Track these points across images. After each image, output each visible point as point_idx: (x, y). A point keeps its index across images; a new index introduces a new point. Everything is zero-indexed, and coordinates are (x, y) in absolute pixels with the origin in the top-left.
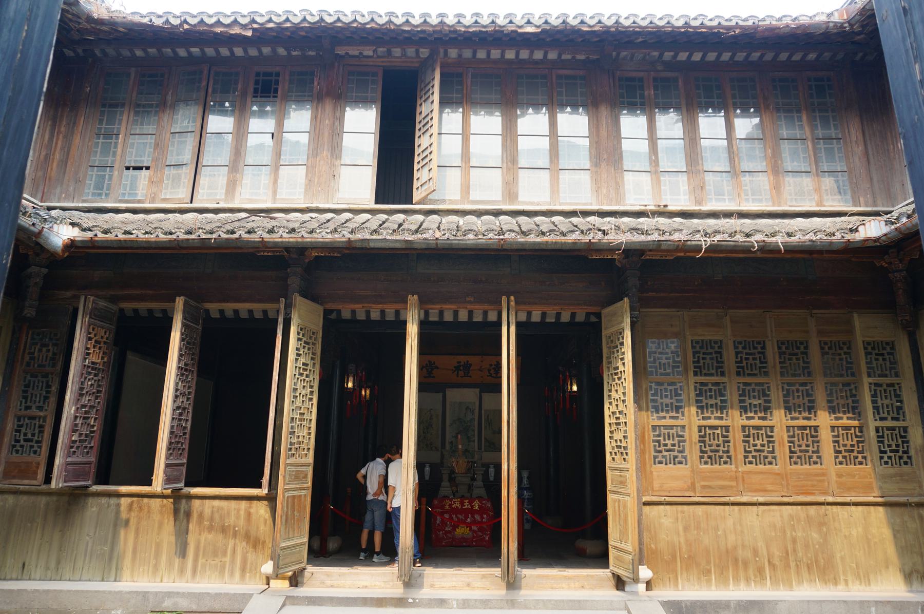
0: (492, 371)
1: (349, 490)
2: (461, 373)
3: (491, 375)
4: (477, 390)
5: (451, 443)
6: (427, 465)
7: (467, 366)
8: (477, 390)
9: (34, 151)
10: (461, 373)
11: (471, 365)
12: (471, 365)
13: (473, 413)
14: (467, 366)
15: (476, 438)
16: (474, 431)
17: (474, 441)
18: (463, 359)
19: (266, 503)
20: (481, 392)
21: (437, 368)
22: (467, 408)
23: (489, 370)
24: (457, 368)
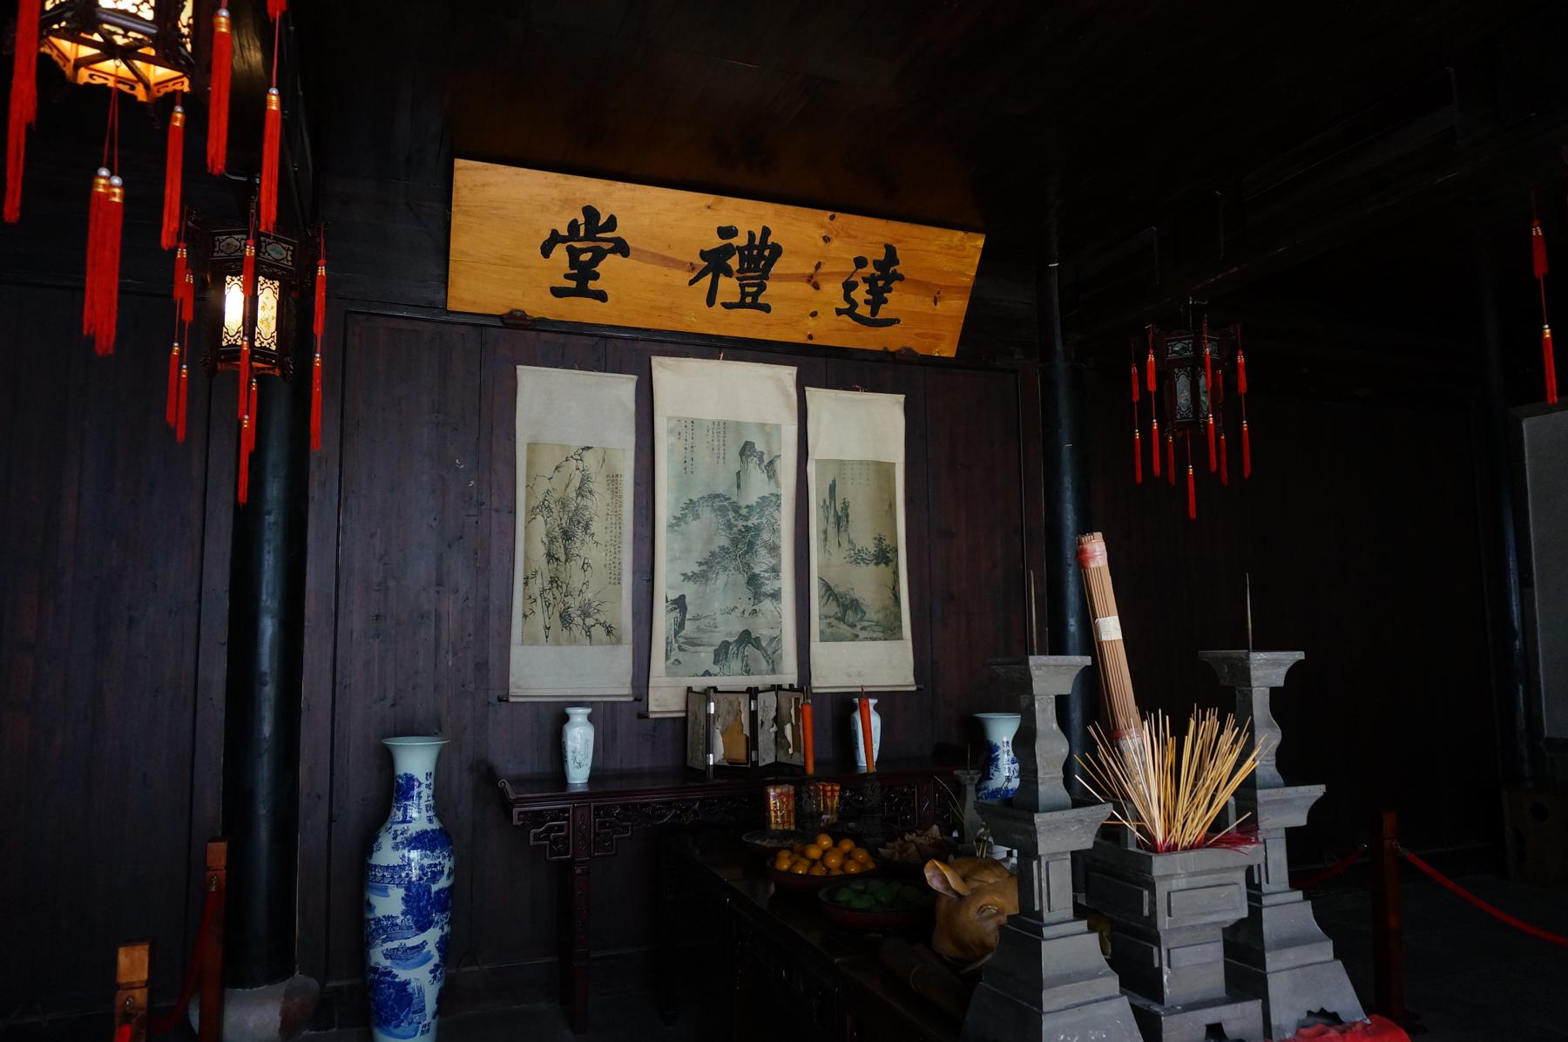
0: (861, 293)
1: (133, 963)
2: (729, 287)
3: (850, 312)
4: (788, 374)
5: (680, 604)
6: (579, 716)
7: (760, 257)
8: (788, 374)
9: (613, 479)
10: (729, 287)
11: (777, 251)
12: (777, 251)
13: (770, 468)
14: (760, 257)
15: (787, 583)
16: (774, 549)
17: (776, 596)
18: (748, 216)
19: (1244, 914)
20: (801, 385)
21: (621, 248)
22: (746, 450)
23: (849, 286)
24: (715, 262)
